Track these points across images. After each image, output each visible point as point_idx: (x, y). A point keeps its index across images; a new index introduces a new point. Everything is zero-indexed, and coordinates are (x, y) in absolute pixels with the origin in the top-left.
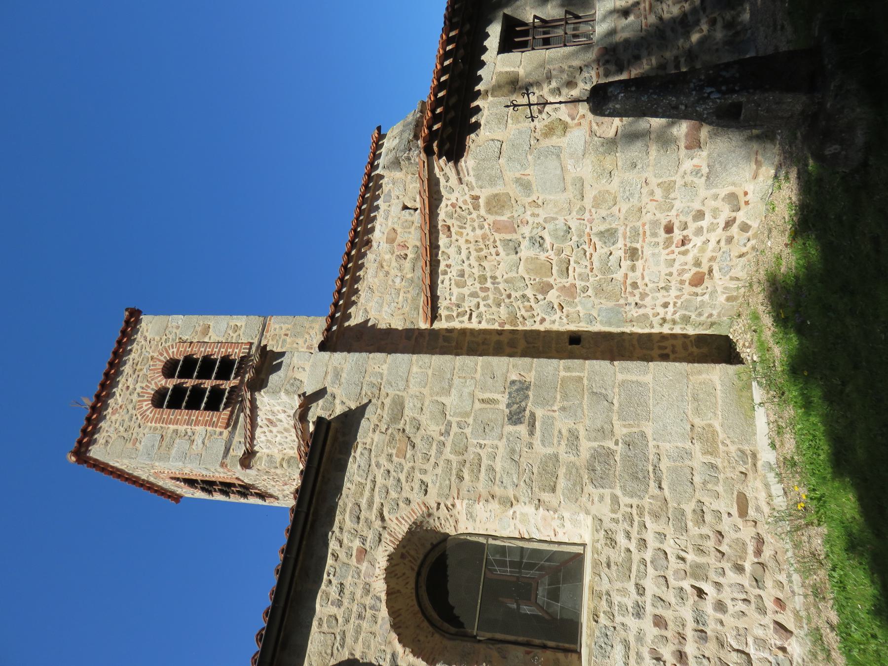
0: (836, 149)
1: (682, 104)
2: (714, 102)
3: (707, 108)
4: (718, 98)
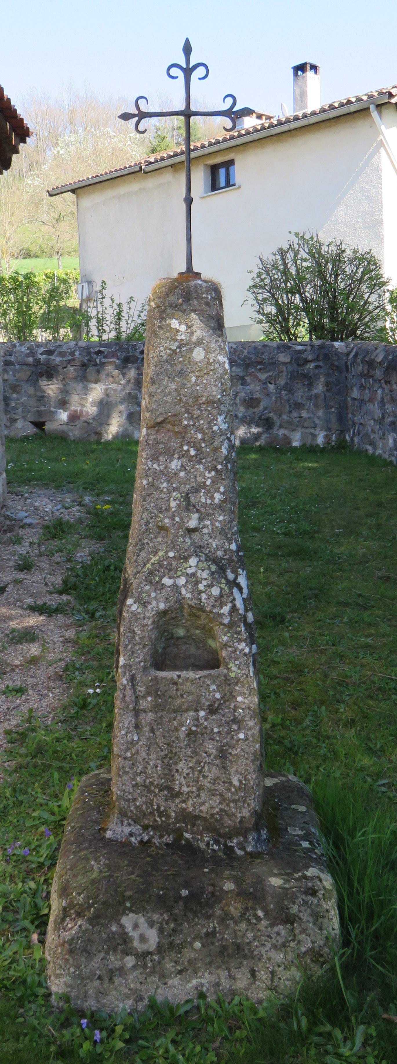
0: (143, 939)
1: (200, 519)
2: (220, 600)
3: (197, 583)
4: (234, 609)
